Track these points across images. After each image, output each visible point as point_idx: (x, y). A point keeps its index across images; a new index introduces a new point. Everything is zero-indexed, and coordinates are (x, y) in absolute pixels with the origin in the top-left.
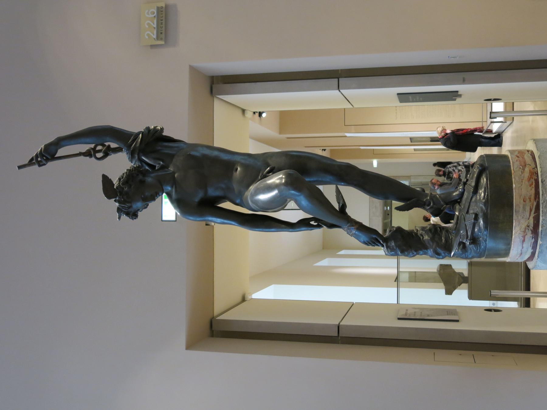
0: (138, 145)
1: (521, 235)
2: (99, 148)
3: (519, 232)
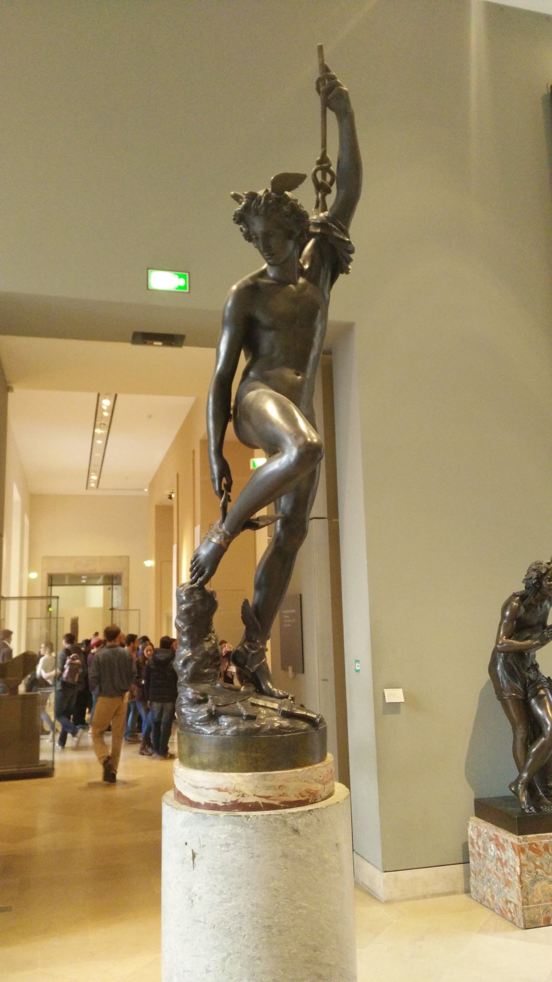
0: (336, 234)
1: (228, 785)
2: (329, 178)
3: (234, 782)
